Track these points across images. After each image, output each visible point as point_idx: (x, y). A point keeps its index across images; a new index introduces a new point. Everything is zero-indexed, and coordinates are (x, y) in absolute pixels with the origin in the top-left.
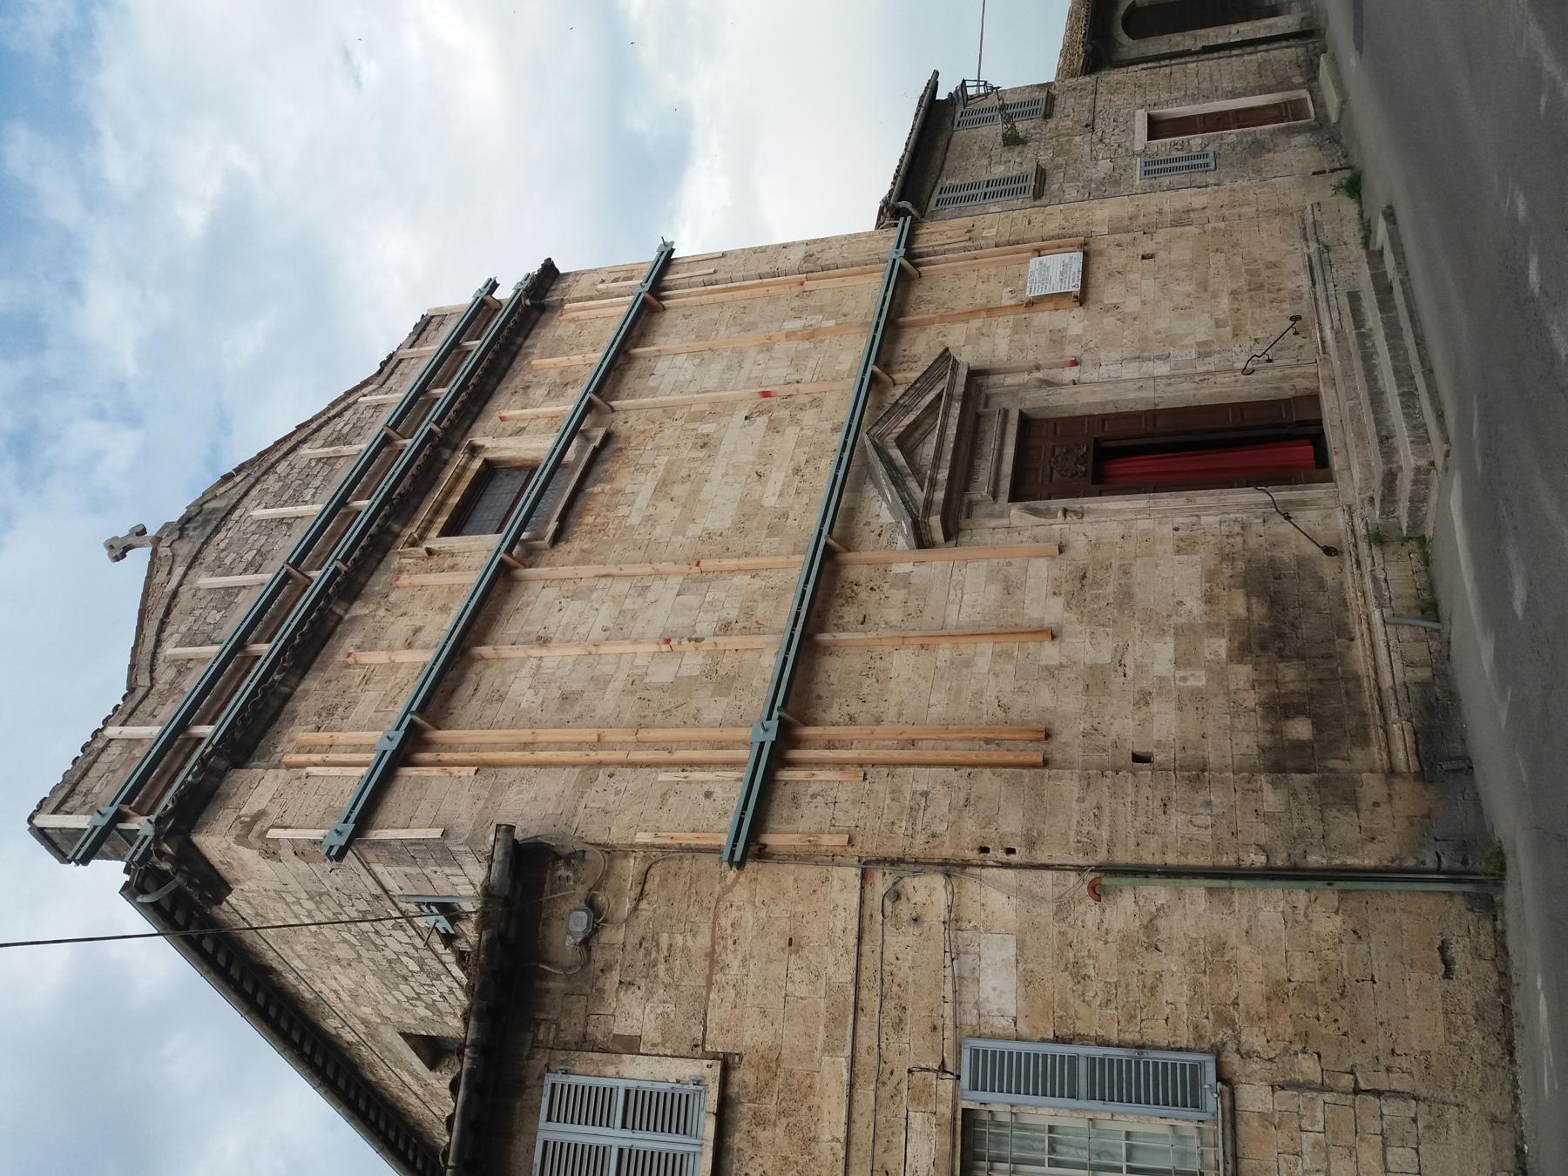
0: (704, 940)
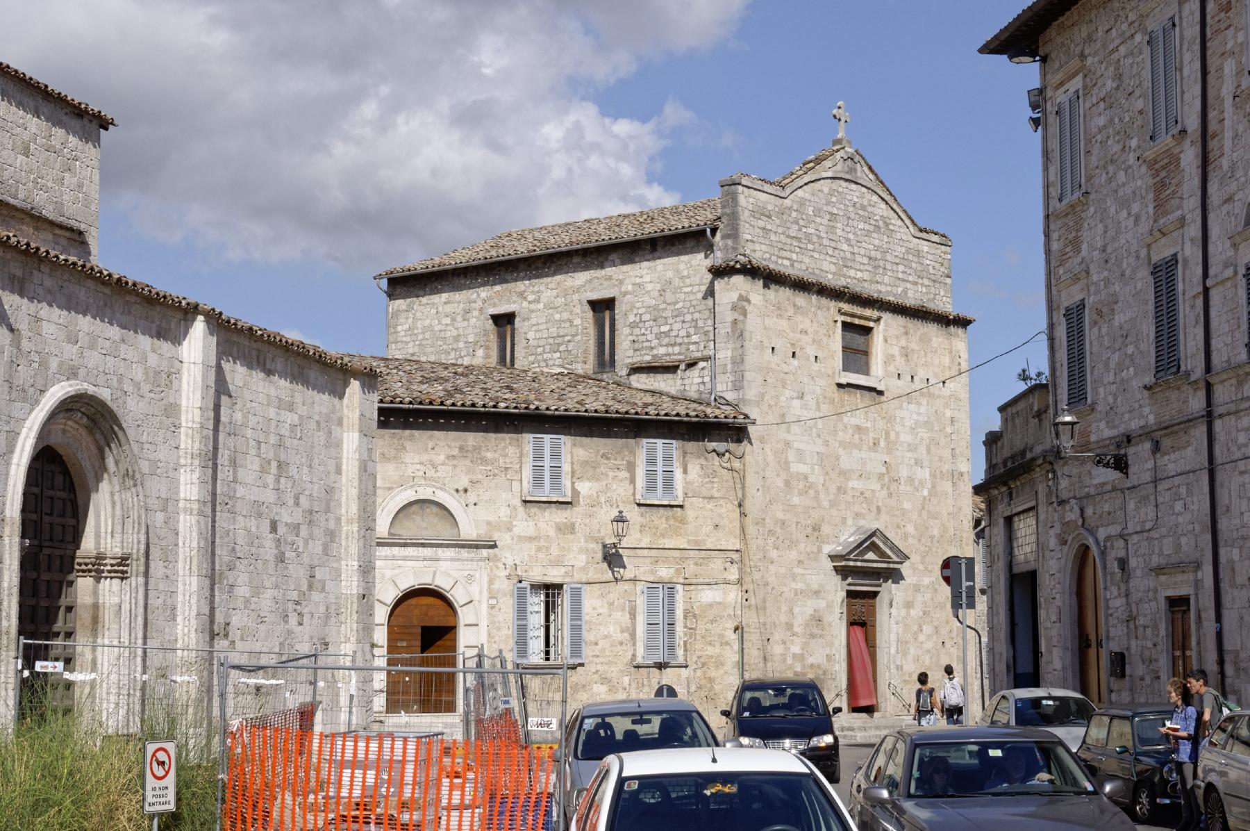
0: (716, 494)
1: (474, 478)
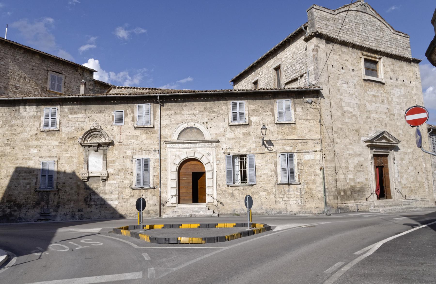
0: (309, 118)
1: (210, 118)
